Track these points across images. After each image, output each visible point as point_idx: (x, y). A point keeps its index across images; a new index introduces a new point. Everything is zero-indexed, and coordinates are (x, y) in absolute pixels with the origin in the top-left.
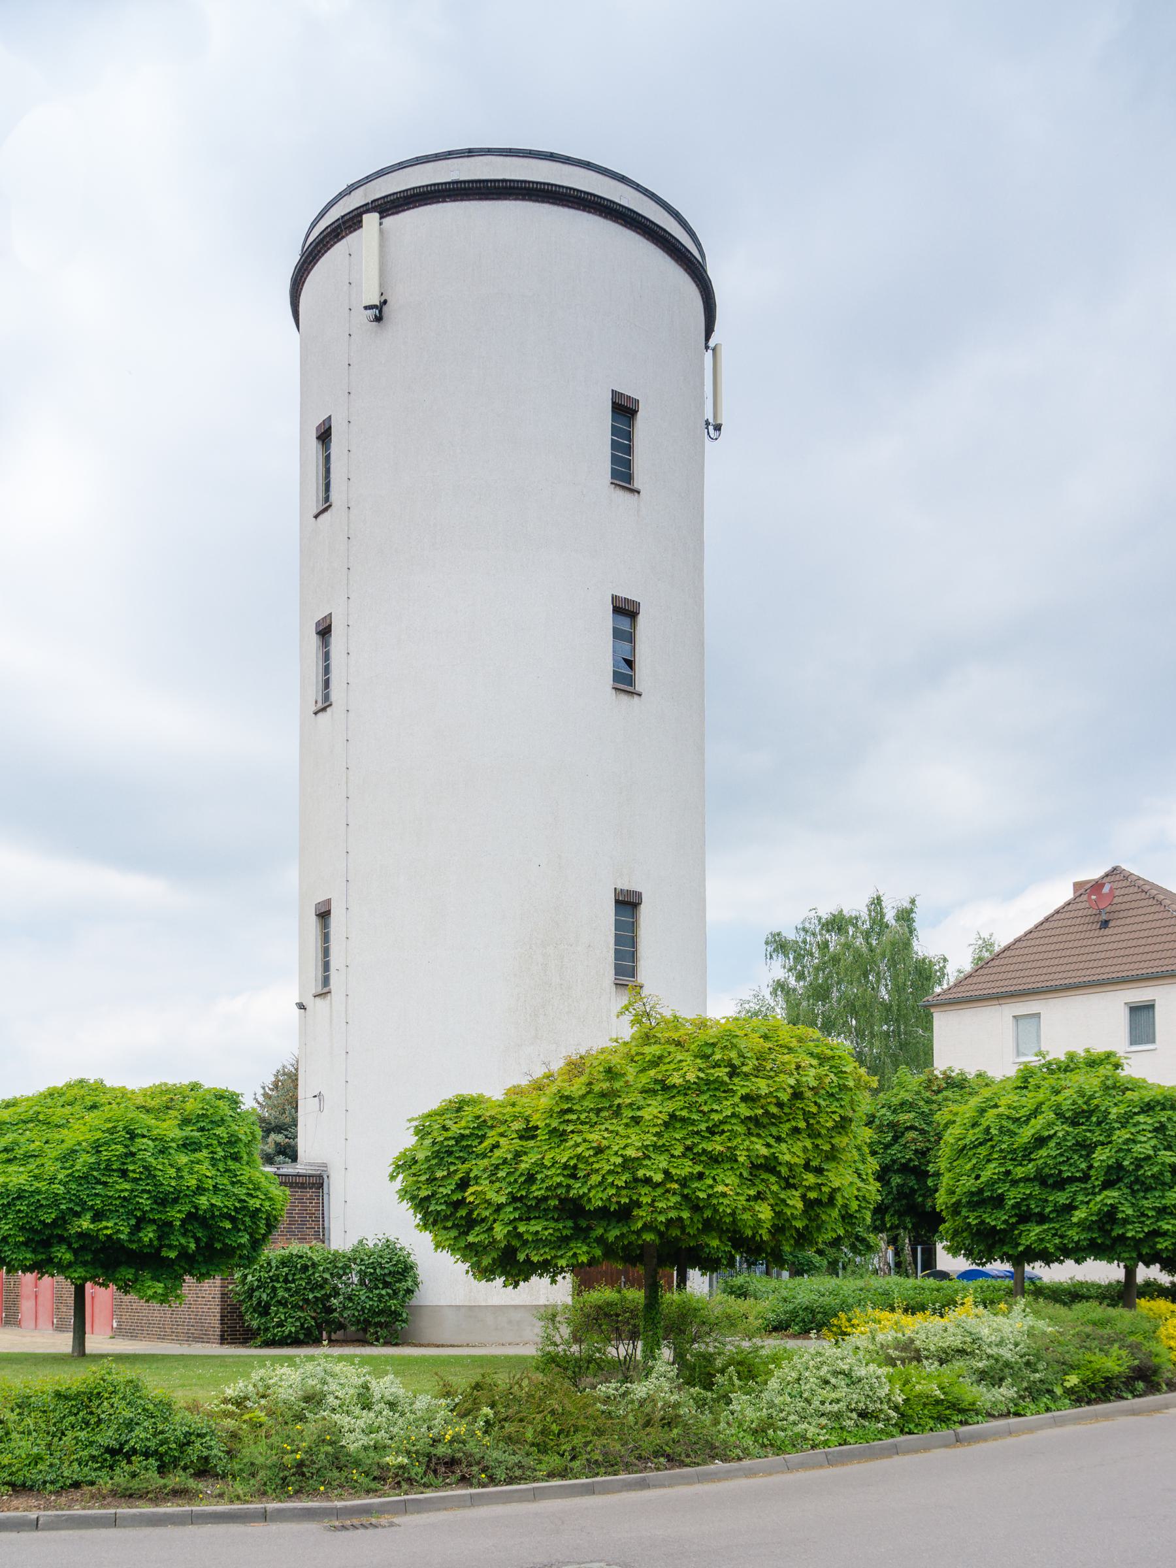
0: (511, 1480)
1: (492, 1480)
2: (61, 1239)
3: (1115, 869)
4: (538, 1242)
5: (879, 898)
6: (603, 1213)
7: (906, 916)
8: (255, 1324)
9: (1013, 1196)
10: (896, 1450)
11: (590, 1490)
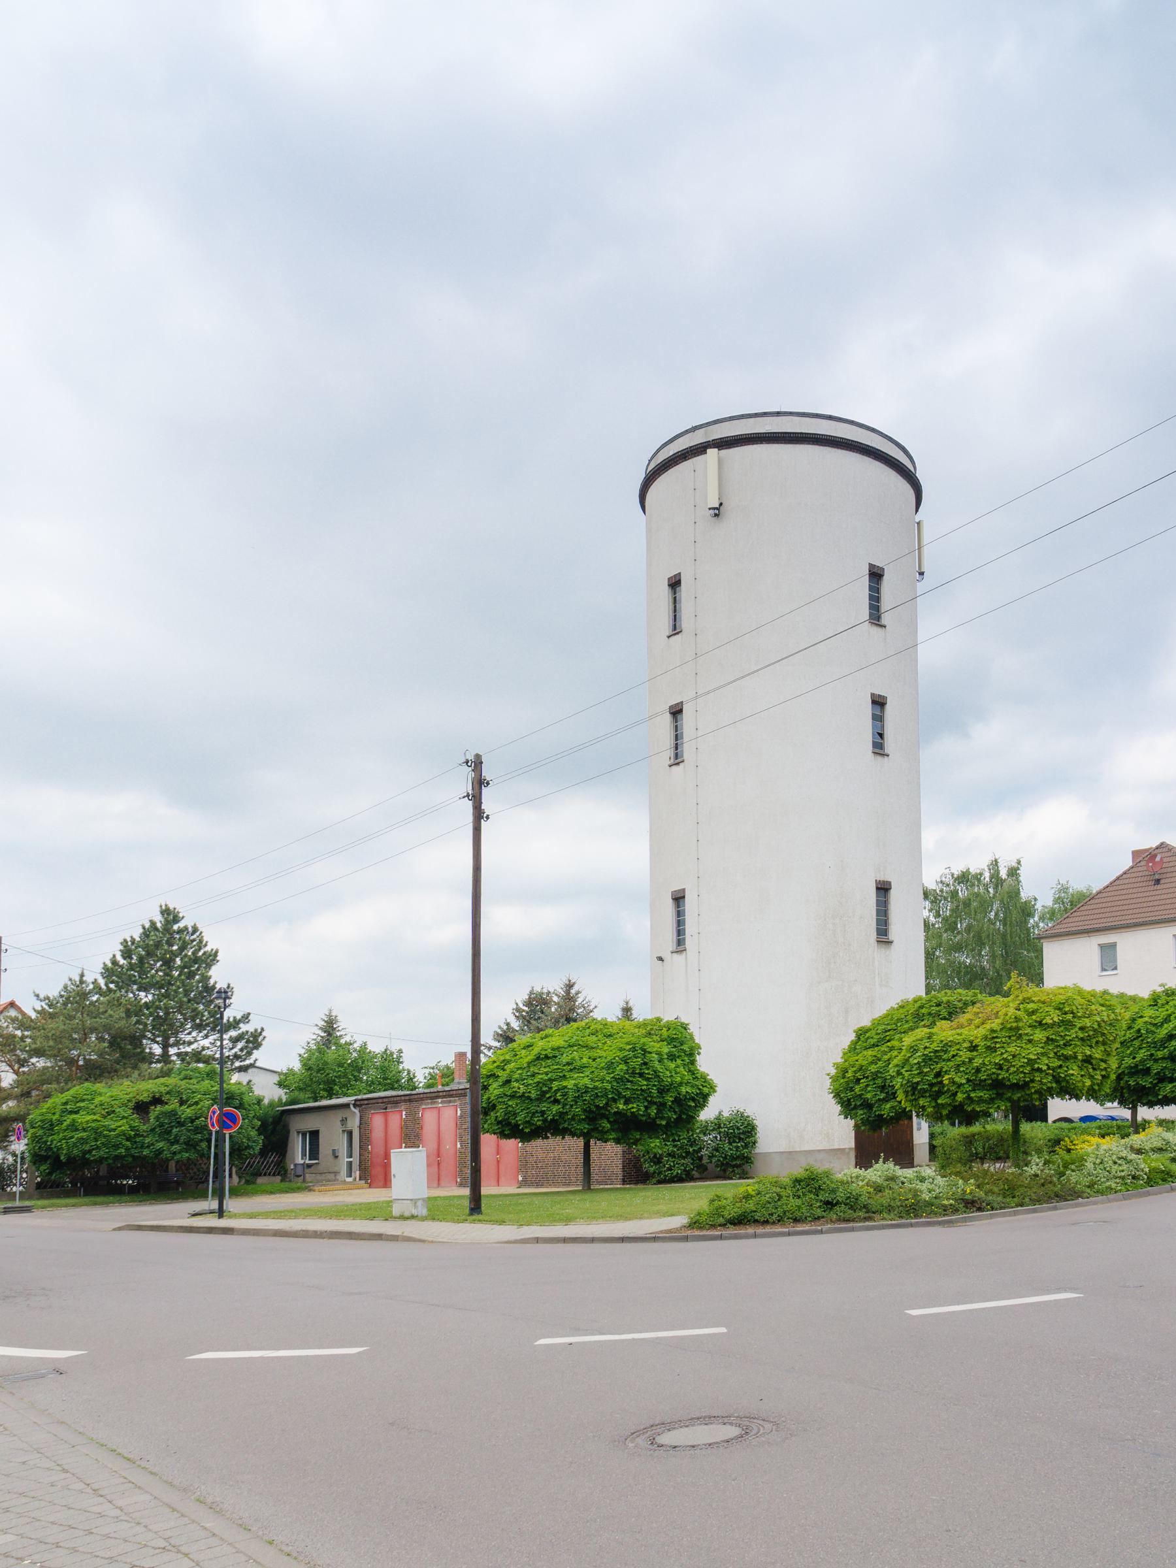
0: (1001, 1208)
1: (992, 1209)
2: (604, 1116)
3: (1162, 844)
4: (981, 1100)
5: (996, 861)
6: (1016, 1087)
7: (1013, 872)
8: (652, 1169)
9: (1156, 1068)
10: (1148, 1194)
11: (1035, 1211)
